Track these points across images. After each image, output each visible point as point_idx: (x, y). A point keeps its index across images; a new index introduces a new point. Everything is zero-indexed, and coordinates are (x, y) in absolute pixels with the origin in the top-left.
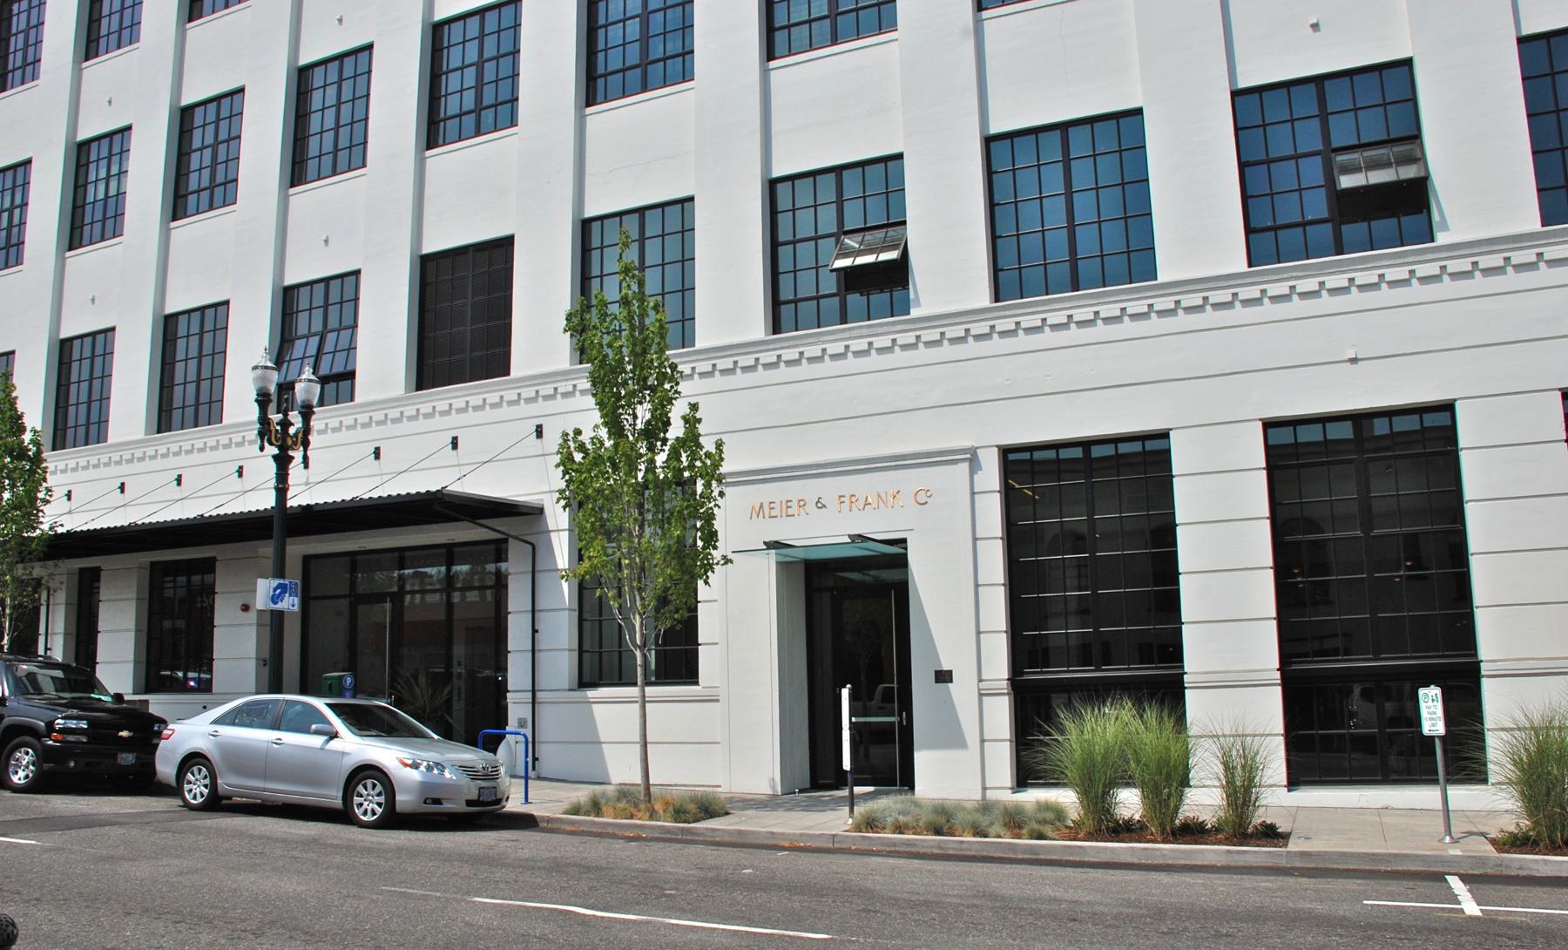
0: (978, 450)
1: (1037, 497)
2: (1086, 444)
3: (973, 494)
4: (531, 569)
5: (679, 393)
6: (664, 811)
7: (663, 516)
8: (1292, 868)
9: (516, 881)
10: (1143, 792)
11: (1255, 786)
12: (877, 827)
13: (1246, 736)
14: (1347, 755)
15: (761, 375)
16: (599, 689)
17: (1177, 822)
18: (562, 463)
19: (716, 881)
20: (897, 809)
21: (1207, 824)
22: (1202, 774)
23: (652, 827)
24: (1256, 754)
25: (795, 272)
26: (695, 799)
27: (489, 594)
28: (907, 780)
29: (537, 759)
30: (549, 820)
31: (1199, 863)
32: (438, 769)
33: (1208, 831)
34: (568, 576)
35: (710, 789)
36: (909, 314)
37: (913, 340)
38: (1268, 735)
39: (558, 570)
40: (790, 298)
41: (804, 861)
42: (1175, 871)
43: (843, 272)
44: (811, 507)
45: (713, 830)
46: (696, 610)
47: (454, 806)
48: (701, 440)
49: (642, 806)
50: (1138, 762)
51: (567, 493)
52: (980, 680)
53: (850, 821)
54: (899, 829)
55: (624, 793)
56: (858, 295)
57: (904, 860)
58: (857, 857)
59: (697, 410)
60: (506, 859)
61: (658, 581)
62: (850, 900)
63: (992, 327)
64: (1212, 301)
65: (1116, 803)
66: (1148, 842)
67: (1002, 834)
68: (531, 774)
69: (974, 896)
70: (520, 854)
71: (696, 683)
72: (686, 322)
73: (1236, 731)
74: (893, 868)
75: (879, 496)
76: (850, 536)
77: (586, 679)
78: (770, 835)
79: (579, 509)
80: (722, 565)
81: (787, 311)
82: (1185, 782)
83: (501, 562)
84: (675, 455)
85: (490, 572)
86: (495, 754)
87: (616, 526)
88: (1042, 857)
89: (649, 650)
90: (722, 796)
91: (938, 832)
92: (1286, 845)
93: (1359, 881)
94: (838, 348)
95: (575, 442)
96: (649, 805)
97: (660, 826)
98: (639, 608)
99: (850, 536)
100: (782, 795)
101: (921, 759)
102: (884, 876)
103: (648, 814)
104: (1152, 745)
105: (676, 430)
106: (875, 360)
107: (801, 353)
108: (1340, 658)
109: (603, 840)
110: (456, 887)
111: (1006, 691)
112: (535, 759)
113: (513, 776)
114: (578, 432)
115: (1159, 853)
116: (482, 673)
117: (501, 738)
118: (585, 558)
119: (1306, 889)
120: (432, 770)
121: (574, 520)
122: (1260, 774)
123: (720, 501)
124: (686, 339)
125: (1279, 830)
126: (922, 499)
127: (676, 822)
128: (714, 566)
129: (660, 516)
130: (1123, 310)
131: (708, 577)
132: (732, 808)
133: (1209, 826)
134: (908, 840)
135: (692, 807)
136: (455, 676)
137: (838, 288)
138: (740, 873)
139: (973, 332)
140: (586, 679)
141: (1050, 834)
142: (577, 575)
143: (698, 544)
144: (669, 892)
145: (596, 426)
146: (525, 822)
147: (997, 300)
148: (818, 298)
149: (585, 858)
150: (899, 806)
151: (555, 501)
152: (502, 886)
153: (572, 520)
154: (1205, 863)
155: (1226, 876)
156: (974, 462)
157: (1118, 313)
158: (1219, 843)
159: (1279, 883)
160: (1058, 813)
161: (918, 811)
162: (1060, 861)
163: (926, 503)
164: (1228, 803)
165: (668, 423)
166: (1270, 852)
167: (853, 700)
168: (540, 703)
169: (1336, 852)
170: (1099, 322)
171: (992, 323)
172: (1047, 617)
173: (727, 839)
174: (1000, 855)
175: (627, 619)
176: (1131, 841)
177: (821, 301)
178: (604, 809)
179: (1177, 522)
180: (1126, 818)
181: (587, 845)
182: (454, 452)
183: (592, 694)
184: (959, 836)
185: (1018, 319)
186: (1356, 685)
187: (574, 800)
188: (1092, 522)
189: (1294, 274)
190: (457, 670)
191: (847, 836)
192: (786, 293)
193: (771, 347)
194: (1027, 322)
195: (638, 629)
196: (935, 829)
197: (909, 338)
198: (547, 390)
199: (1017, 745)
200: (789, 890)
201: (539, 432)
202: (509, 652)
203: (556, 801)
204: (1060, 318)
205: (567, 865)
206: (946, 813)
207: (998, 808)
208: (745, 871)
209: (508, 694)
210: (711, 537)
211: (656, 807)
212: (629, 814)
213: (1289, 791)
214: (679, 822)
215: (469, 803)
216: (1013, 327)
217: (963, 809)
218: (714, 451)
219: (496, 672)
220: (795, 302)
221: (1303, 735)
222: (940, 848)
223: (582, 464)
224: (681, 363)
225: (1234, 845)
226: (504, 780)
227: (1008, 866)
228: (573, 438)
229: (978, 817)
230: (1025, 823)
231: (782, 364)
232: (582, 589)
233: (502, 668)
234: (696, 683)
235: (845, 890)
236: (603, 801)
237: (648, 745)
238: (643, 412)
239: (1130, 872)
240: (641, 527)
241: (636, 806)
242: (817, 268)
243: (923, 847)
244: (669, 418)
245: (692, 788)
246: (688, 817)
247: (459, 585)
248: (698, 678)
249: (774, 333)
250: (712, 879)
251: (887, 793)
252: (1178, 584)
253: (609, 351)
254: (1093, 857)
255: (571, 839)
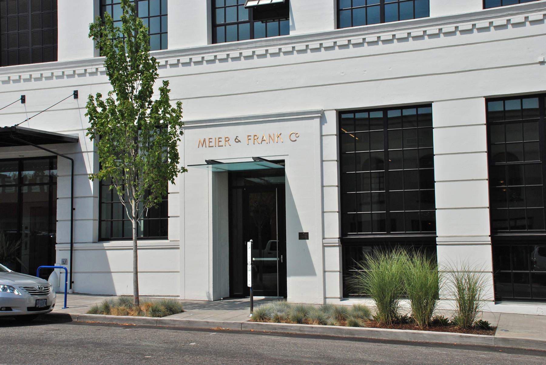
0: (325, 112)
1: (357, 138)
2: (385, 109)
3: (322, 136)
4: (71, 174)
5: (158, 75)
6: (147, 311)
7: (149, 145)
8: (497, 347)
9: (56, 354)
10: (412, 301)
11: (475, 300)
12: (266, 319)
13: (470, 272)
14: (529, 285)
15: (205, 67)
16: (110, 242)
17: (432, 319)
18: (89, 113)
19: (174, 350)
20: (277, 308)
21: (448, 321)
22: (445, 292)
23: (139, 320)
24: (476, 283)
25: (225, 7)
26: (164, 304)
27: (46, 188)
28: (283, 293)
29: (73, 282)
30: (79, 317)
31: (444, 342)
32: (10, 290)
33: (450, 324)
34: (93, 177)
35: (173, 298)
36: (289, 34)
37: (291, 49)
38: (483, 272)
39: (87, 174)
40: (222, 23)
41: (225, 338)
42: (430, 346)
43: (252, 9)
44: (232, 142)
45: (174, 321)
46: (167, 197)
47: (19, 311)
48: (170, 102)
49: (134, 308)
50: (409, 284)
51: (93, 130)
52: (324, 238)
53: (251, 315)
54: (278, 320)
55: (124, 300)
56: (260, 22)
57: (280, 337)
58: (254, 335)
59: (168, 85)
60: (51, 340)
61: (145, 182)
62: (250, 359)
63: (335, 43)
64: (460, 29)
65: (397, 307)
66: (415, 329)
67: (334, 323)
68: (69, 290)
69: (319, 358)
70: (60, 338)
71: (167, 239)
72: (162, 35)
73: (465, 269)
74: (274, 342)
75: (270, 136)
76: (253, 158)
77: (103, 236)
78: (206, 324)
79: (100, 140)
80: (182, 172)
81: (220, 30)
82: (436, 296)
83: (53, 169)
84: (155, 110)
85: (47, 176)
86: (47, 280)
87: (121, 150)
88: (356, 336)
89: (140, 220)
90: (180, 302)
91: (299, 322)
92: (494, 334)
93: (537, 357)
94: (249, 52)
95: (97, 101)
96: (138, 307)
97: (143, 319)
98: (134, 196)
99: (253, 158)
100: (213, 301)
101: (291, 281)
102: (269, 346)
103: (137, 313)
104: (417, 275)
105: (156, 96)
106: (269, 60)
107: (228, 55)
108: (526, 230)
109: (110, 328)
110: (17, 360)
111: (338, 244)
112: (71, 282)
113: (58, 292)
114: (99, 95)
115: (421, 336)
116: (40, 233)
117: (51, 271)
118: (103, 167)
119: (506, 360)
120: (7, 290)
121: (97, 146)
122: (478, 294)
123: (181, 137)
124: (163, 44)
125: (490, 326)
126: (294, 138)
127: (153, 317)
128: (177, 173)
129: (147, 145)
130: (409, 34)
131: (174, 179)
132: (186, 308)
133: (450, 321)
134: (283, 326)
135: (162, 308)
136: (23, 235)
137: (249, 18)
138: (189, 345)
139: (324, 45)
140: (103, 236)
141: (361, 324)
142: (99, 177)
143: (169, 161)
144: (147, 357)
145: (110, 93)
146: (65, 319)
147: (338, 27)
148: (238, 23)
149: (100, 338)
150: (278, 307)
151: (85, 134)
152: (47, 357)
153: (96, 145)
154: (448, 342)
155: (460, 350)
156: (322, 119)
157: (406, 36)
158: (455, 331)
159: (490, 355)
160: (365, 312)
161: (288, 310)
162: (366, 339)
163: (296, 140)
164: (461, 309)
165: (152, 92)
166: (484, 337)
167: (253, 249)
168: (75, 250)
169: (523, 339)
170: (395, 41)
171: (335, 40)
172: (361, 205)
173: (182, 326)
174: (333, 335)
175: (127, 203)
176: (406, 329)
177: (240, 25)
178: (112, 310)
179: (434, 153)
180: (403, 316)
181: (100, 331)
182: (23, 104)
183: (106, 244)
184: (311, 324)
185: (349, 38)
186: (536, 246)
187: (94, 305)
188: (387, 153)
189: (510, 12)
190: (25, 232)
191: (249, 324)
192: (220, 20)
193: (211, 51)
194: (355, 40)
195: (133, 208)
196: (297, 320)
197: (289, 48)
198: (80, 70)
199: (343, 274)
200: (215, 354)
201: (76, 95)
202: (57, 221)
203: (83, 306)
204: (373, 38)
205: (89, 343)
206: (304, 311)
207: (332, 309)
208: (191, 344)
209: (56, 245)
210: (175, 157)
211: (142, 309)
212: (126, 313)
213: (496, 304)
214: (155, 317)
215: (29, 309)
216: (346, 43)
217: (313, 309)
218: (176, 108)
219: (49, 233)
220: (225, 25)
221: (503, 273)
222: (300, 331)
223: (102, 114)
224: (159, 58)
225: (464, 333)
226: (52, 294)
227: (337, 341)
228: (96, 99)
229: (321, 313)
230: (347, 317)
231: (217, 61)
232: (102, 185)
233: (53, 230)
234: (167, 239)
235: (247, 354)
236: (111, 306)
237: (138, 273)
238: (138, 85)
239: (405, 346)
240: (136, 151)
241: (130, 308)
242: (237, 6)
243: (291, 330)
244: (152, 89)
245: (162, 298)
246: (161, 313)
247: (27, 183)
248: (168, 236)
249: (213, 43)
250: (172, 348)
251: (271, 300)
252: (433, 187)
253: (116, 49)
254: (385, 337)
255: (91, 328)
